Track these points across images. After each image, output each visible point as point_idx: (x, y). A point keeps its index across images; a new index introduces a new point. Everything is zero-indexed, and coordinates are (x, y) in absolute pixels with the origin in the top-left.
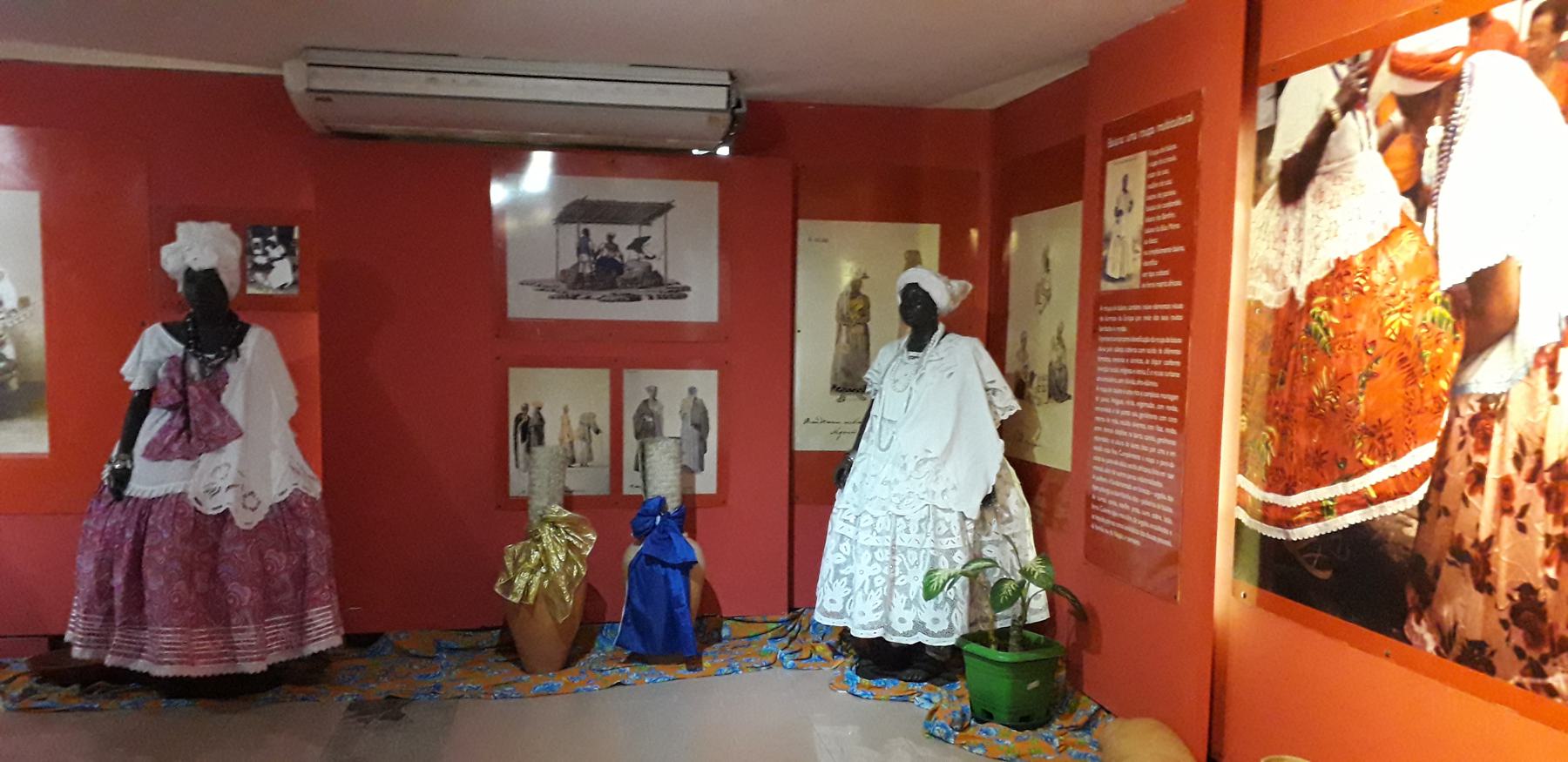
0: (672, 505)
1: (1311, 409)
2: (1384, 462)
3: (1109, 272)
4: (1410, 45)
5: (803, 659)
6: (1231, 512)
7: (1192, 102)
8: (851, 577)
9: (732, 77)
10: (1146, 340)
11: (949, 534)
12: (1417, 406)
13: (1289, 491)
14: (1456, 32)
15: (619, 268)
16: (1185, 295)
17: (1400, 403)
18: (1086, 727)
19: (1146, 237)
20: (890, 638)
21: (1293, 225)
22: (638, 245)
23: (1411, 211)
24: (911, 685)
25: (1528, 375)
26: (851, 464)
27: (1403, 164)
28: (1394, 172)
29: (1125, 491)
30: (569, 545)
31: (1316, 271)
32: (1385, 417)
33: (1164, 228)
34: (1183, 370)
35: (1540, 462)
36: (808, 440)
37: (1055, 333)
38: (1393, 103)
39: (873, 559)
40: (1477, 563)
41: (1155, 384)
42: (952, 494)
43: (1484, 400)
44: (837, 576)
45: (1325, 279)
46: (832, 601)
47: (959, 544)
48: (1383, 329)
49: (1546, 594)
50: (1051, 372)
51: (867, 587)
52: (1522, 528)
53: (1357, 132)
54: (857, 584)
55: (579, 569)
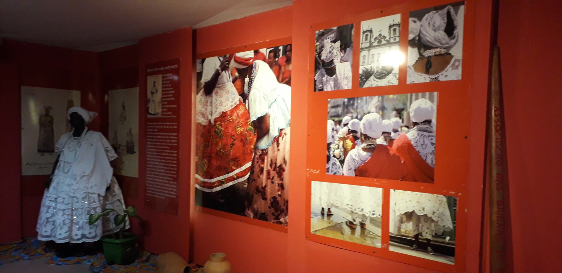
1: (217, 154)
2: (238, 168)
3: (150, 111)
4: (239, 55)
6: (194, 185)
7: (176, 61)
8: (54, 222)
10: (165, 134)
11: (94, 202)
12: (246, 152)
13: (211, 178)
14: (250, 54)
16: (178, 120)
17: (241, 152)
18: (147, 261)
19: (163, 101)
21: (209, 101)
23: (242, 100)
24: (81, 258)
25: (272, 144)
26: (51, 179)
27: (239, 87)
28: (237, 89)
29: (159, 182)
31: (216, 115)
32: (238, 155)
33: (169, 99)
34: (178, 143)
35: (276, 165)
36: (28, 171)
37: (128, 131)
38: (235, 70)
39: (64, 214)
40: (262, 192)
41: (168, 148)
42: (95, 188)
43: (263, 150)
45: (219, 117)
46: (46, 231)
47: (98, 205)
48: (236, 132)
49: (279, 198)
51: (62, 225)
52: (272, 182)
53: (226, 76)
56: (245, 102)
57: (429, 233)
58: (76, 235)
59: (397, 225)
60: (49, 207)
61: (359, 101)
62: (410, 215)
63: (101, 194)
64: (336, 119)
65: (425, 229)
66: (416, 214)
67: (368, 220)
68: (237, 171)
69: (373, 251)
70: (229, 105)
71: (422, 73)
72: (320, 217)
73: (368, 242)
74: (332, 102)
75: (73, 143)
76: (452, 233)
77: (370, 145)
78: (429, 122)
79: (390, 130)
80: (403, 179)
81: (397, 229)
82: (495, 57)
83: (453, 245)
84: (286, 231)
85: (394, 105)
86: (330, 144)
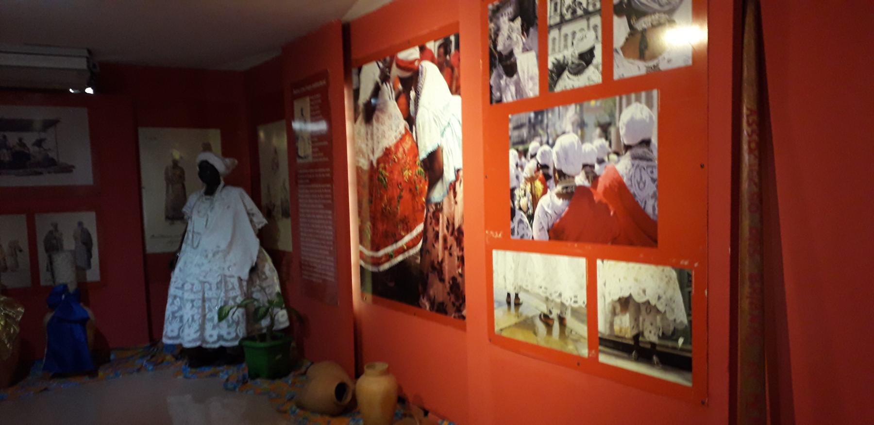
0: (72, 288)
4: (403, 55)
5: (158, 365)
7: (323, 75)
8: (181, 317)
9: (89, 52)
14: (413, 53)
15: (27, 156)
20: (204, 346)
22: (39, 143)
27: (404, 107)
30: (7, 316)
31: (379, 153)
36: (154, 247)
39: (193, 306)
40: (438, 268)
43: (436, 204)
44: (174, 317)
48: (403, 176)
50: (282, 203)
52: (451, 254)
53: (387, 90)
54: (185, 318)
55: (14, 329)
56: (411, 129)
57: (653, 332)
58: (211, 336)
59: (608, 320)
60: (175, 297)
61: (550, 115)
62: (625, 303)
63: (242, 277)
64: (521, 148)
65: (647, 324)
66: (634, 300)
67: (569, 312)
68: (407, 238)
69: (576, 362)
70: (393, 137)
71: (634, 58)
72: (506, 307)
73: (570, 348)
74: (514, 119)
75: (205, 205)
76: (687, 332)
77: (567, 188)
78: (646, 143)
79: (592, 160)
80: (615, 241)
81: (608, 326)
82: (750, 20)
83: (690, 351)
84: (464, 328)
85: (596, 118)
86: (513, 190)
